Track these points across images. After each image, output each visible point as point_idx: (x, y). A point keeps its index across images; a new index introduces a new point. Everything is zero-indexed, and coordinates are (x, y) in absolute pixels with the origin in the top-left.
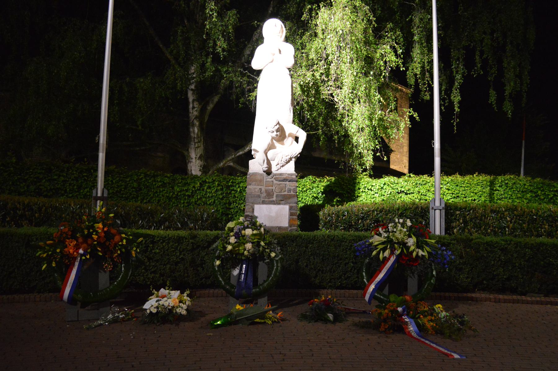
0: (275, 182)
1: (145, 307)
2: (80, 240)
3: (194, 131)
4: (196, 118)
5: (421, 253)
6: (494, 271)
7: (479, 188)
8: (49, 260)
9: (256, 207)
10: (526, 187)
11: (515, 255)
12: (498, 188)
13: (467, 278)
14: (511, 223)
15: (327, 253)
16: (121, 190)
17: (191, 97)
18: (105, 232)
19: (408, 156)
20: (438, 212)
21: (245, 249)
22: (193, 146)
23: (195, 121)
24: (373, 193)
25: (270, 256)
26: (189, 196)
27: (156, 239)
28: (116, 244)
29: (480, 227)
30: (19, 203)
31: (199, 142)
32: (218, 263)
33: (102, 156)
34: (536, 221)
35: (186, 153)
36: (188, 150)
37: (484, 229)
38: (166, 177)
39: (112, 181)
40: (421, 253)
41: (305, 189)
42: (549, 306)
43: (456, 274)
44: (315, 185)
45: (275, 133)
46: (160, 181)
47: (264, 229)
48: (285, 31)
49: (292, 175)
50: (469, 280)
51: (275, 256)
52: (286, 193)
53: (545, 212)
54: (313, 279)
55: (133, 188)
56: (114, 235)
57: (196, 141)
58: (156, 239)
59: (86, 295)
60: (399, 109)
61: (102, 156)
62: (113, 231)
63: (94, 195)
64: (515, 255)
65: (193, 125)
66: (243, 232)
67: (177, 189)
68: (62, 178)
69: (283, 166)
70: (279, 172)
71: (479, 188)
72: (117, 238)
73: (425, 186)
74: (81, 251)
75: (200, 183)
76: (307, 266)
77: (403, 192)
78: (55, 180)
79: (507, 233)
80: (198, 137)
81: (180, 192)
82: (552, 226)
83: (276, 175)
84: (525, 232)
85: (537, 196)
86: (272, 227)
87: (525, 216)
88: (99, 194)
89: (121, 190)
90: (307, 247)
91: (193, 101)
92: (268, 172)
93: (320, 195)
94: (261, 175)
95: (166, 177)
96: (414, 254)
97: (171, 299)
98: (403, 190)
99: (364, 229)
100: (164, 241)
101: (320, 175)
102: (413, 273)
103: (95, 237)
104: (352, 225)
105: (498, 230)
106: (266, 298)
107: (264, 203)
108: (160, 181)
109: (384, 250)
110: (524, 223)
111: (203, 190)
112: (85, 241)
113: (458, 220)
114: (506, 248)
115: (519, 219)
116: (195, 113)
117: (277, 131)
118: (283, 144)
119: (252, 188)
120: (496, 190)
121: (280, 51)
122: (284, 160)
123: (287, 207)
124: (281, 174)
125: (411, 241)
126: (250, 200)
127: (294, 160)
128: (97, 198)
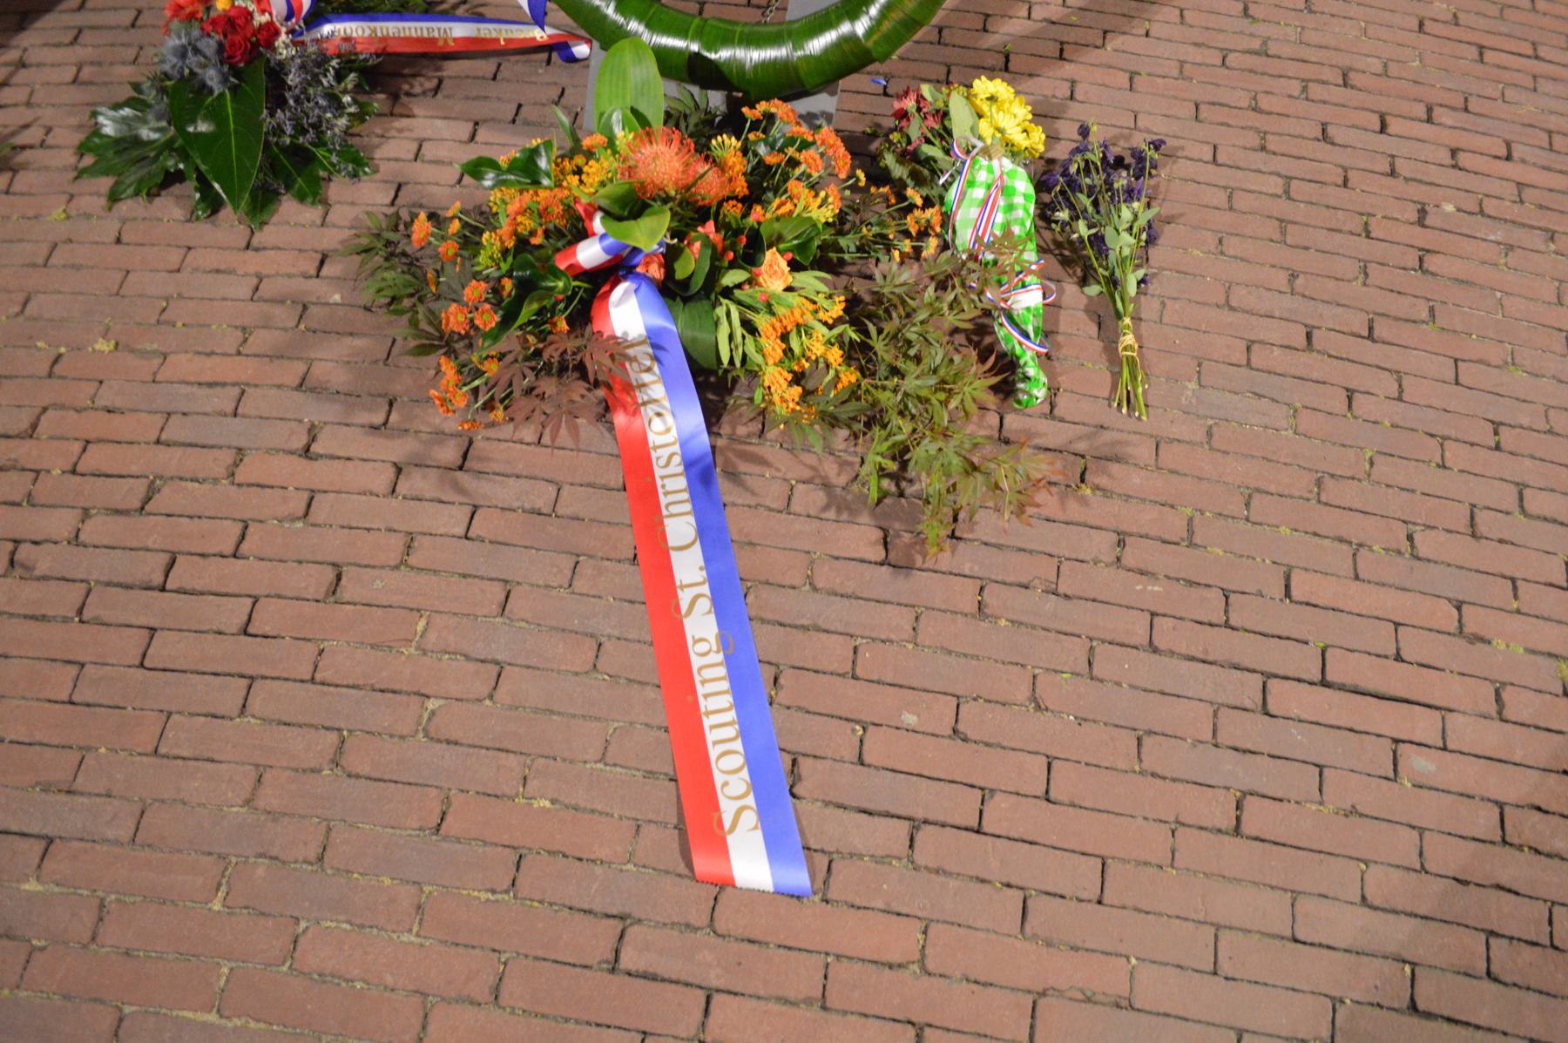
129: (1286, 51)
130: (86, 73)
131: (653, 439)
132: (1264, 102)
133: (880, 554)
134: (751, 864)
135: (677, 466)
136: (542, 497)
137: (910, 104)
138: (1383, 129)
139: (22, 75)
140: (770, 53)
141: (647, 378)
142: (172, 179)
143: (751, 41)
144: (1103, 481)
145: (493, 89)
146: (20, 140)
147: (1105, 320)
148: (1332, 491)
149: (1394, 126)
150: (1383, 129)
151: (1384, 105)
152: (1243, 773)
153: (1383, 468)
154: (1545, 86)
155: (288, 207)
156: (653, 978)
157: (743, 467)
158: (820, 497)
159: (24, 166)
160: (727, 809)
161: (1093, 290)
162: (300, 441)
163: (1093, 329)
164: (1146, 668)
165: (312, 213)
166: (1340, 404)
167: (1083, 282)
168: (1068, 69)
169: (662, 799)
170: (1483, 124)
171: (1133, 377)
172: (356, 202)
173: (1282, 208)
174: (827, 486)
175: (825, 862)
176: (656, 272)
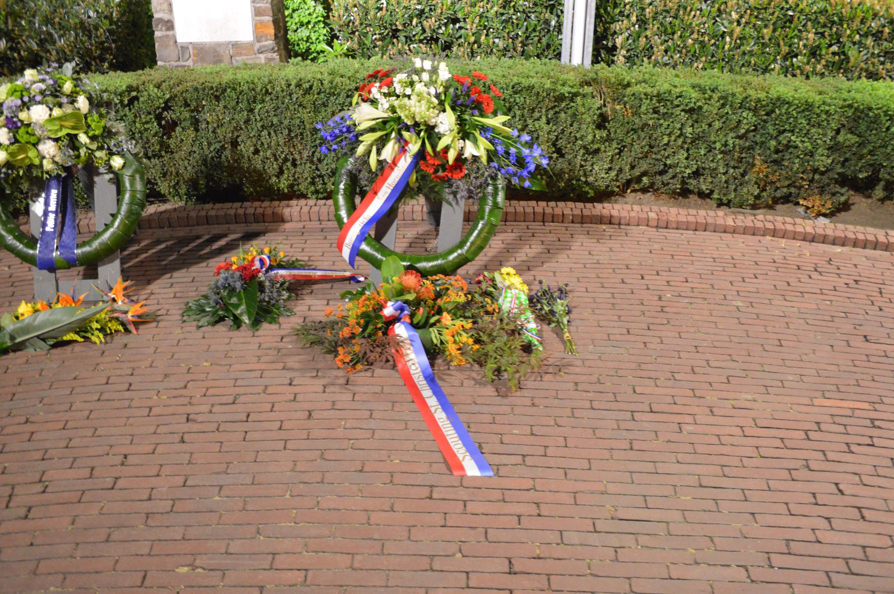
5: (470, 150)
6: (668, 157)
11: (717, 125)
14: (739, 24)
15: (298, 122)
29: (673, 34)
34: (791, 22)
37: (681, 37)
42: (769, 238)
43: (586, 161)
47: (90, 99)
50: (613, 174)
54: (274, 179)
64: (717, 125)
66: (23, 115)
76: (256, 152)
79: (727, 47)
82: (822, 35)
84: (764, 45)
86: (219, 45)
87: (771, 11)
90: (251, 111)
96: (452, 156)
99: (425, 38)
102: (455, 194)
104: (397, 30)
105: (709, 41)
109: (381, 143)
110: (766, 26)
113: (628, 16)
114: (700, 108)
115: (756, 17)
125: (446, 122)
129: (606, 262)
130: (178, 295)
131: (412, 372)
132: (601, 275)
133: (496, 394)
134: (472, 469)
135: (422, 378)
136: (378, 389)
137: (481, 278)
138: (643, 278)
139: (153, 296)
140: (435, 263)
141: (408, 352)
142: (222, 319)
143: (428, 260)
144: (567, 371)
145: (331, 291)
146: (159, 313)
147: (559, 332)
148: (643, 366)
149: (646, 277)
150: (643, 278)
151: (642, 272)
152: (630, 435)
153: (659, 360)
154: (695, 263)
155: (265, 325)
156: (445, 499)
157: (444, 377)
158: (473, 382)
159: (162, 320)
160: (460, 457)
161: (553, 325)
162: (289, 382)
163: (555, 336)
164: (592, 414)
165: (274, 326)
166: (642, 346)
167: (549, 324)
168: (532, 273)
169: (438, 457)
170: (677, 274)
171: (571, 345)
172: (289, 323)
173: (612, 301)
174: (474, 379)
175: (497, 468)
176: (408, 320)
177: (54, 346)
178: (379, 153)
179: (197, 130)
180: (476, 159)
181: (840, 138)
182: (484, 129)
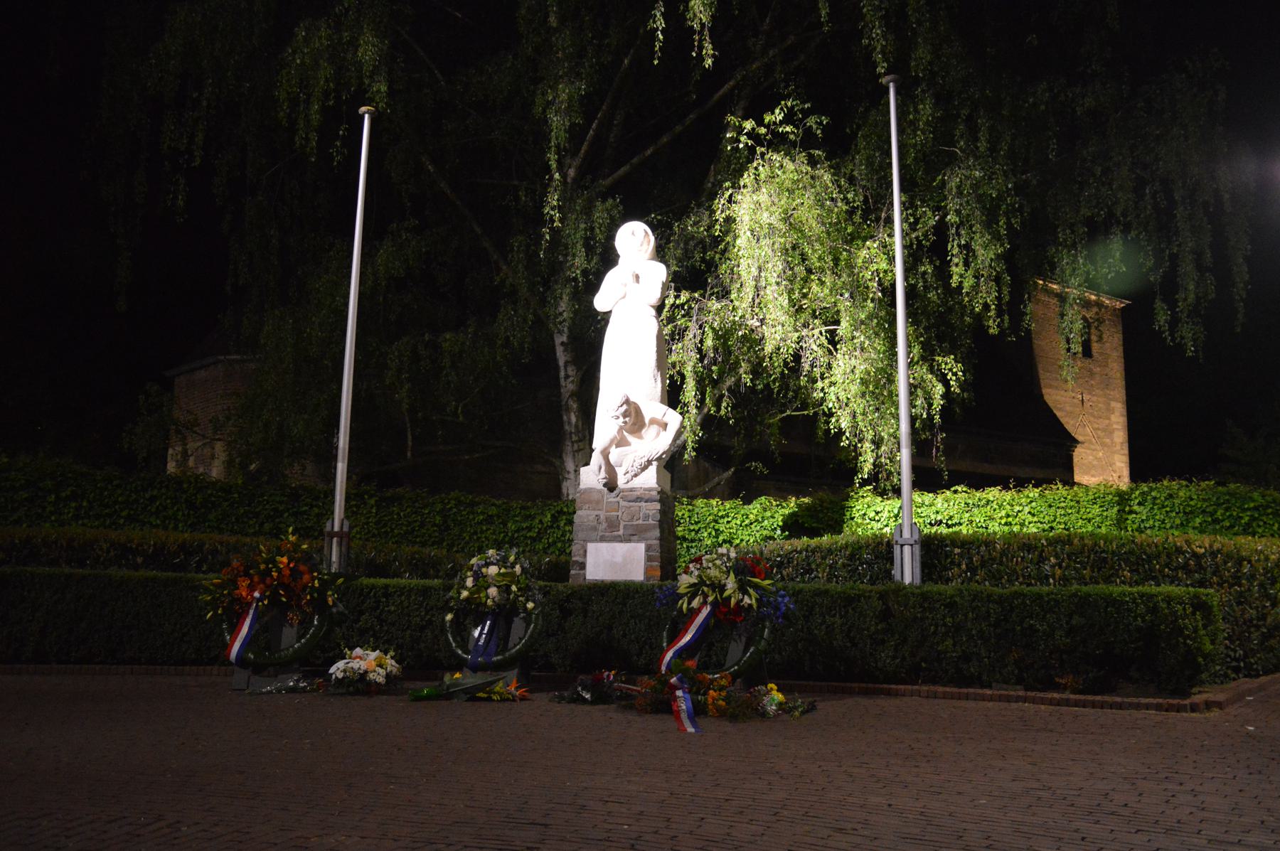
0: (623, 503)
1: (331, 671)
2: (256, 579)
3: (569, 419)
4: (573, 394)
5: (747, 600)
7: (1096, 510)
8: (214, 604)
9: (591, 547)
10: (1192, 503)
12: (1136, 508)
13: (894, 658)
16: (413, 530)
17: (562, 357)
18: (291, 570)
19: (1126, 451)
20: (907, 549)
21: (488, 597)
22: (569, 448)
23: (571, 402)
24: (879, 525)
25: (526, 608)
26: (533, 539)
27: (391, 590)
28: (306, 586)
30: (221, 543)
31: (580, 441)
32: (449, 617)
33: (341, 467)
35: (558, 463)
36: (561, 457)
38: (494, 505)
39: (398, 514)
40: (747, 600)
41: (747, 522)
44: (768, 514)
45: (621, 419)
46: (482, 513)
48: (652, 238)
49: (650, 490)
51: (534, 608)
52: (640, 522)
53: (1123, 545)
55: (435, 525)
56: (302, 573)
57: (574, 438)
58: (391, 590)
59: (263, 658)
60: (1095, 347)
61: (341, 467)
62: (302, 568)
63: (328, 528)
65: (568, 410)
66: (484, 570)
67: (511, 526)
68: (316, 510)
69: (636, 475)
70: (630, 485)
71: (1096, 510)
72: (306, 577)
73: (983, 510)
74: (257, 594)
75: (553, 516)
76: (624, 635)
77: (941, 522)
78: (305, 513)
80: (577, 432)
81: (517, 531)
82: (1137, 571)
83: (623, 491)
85: (1216, 521)
88: (336, 528)
89: (413, 530)
91: (566, 363)
92: (611, 485)
93: (779, 532)
94: (600, 491)
95: (494, 505)
97: (366, 661)
98: (939, 518)
100: (402, 594)
101: (782, 495)
103: (275, 574)
106: (516, 671)
107: (603, 539)
108: (482, 513)
111: (558, 527)
112: (263, 581)
113: (959, 565)
116: (571, 387)
117: (625, 415)
118: (641, 437)
119: (583, 516)
120: (1131, 512)
121: (637, 277)
122: (637, 464)
123: (641, 547)
124: (632, 490)
125: (731, 583)
126: (579, 535)
127: (655, 463)
128: (332, 535)
177: (469, 700)
178: (689, 603)
179: (585, 617)
180: (750, 605)
181: (1074, 622)
182: (756, 587)
